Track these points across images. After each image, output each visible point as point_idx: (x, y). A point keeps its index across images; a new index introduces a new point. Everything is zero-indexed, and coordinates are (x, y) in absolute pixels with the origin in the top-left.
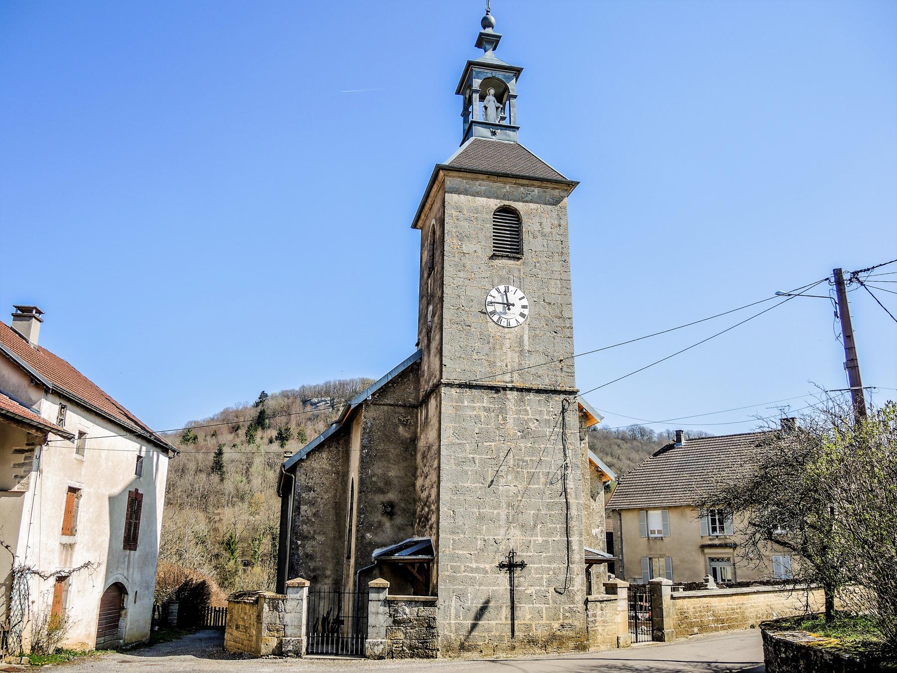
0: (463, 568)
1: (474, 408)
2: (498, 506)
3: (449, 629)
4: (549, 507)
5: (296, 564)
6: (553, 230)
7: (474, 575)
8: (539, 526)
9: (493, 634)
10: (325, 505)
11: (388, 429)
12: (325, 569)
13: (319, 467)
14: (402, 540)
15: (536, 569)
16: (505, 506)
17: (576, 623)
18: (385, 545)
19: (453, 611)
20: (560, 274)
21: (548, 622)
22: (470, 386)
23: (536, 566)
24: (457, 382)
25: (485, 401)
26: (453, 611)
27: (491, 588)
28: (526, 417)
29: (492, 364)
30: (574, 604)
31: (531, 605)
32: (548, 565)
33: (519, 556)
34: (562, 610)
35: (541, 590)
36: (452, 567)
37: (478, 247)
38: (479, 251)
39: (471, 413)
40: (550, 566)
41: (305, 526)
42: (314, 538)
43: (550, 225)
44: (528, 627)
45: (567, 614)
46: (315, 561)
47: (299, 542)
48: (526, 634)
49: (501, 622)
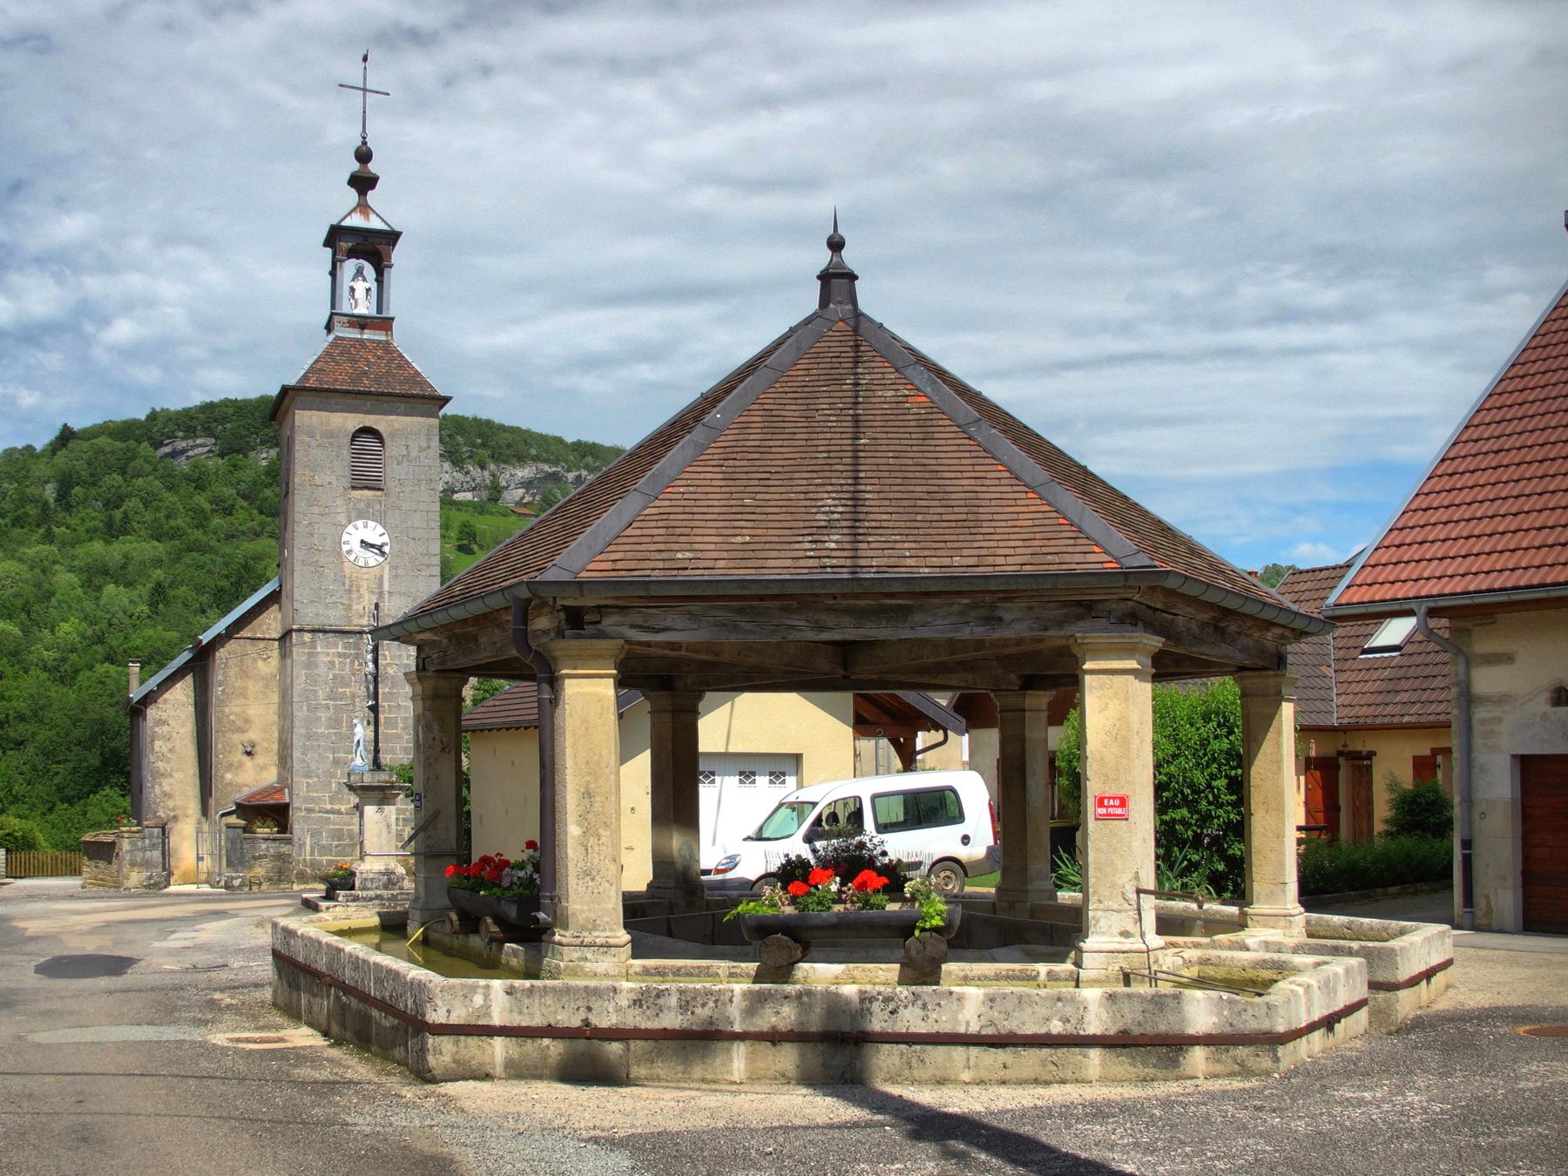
1: (328, 654)
10: (182, 739)
12: (186, 808)
19: (308, 848)
24: (310, 627)
26: (308, 848)
29: (349, 607)
37: (333, 479)
38: (334, 482)
41: (160, 763)
42: (171, 776)
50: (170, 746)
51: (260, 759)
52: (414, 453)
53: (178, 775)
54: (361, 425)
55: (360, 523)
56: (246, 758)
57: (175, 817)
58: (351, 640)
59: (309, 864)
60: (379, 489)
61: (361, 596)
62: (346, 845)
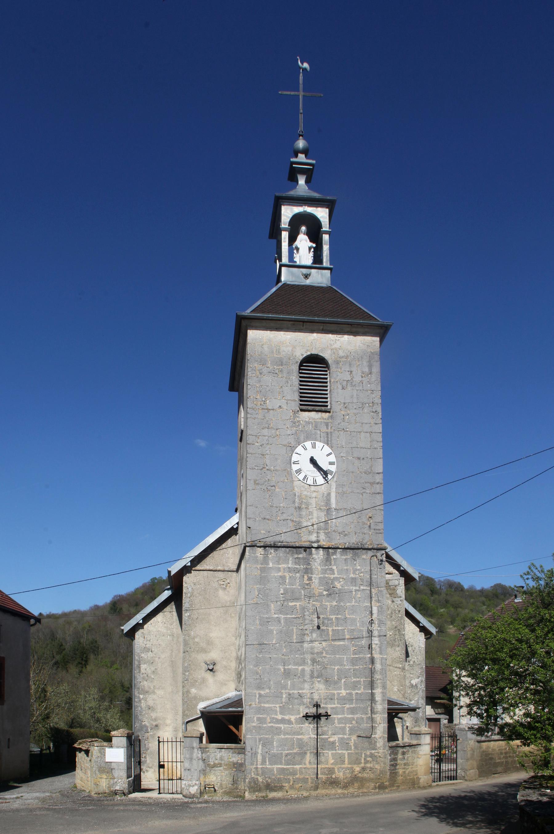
0: (268, 720)
1: (279, 570)
2: (303, 662)
3: (256, 773)
4: (354, 662)
5: (140, 714)
6: (364, 379)
7: (279, 725)
8: (343, 681)
9: (297, 776)
11: (208, 593)
13: (155, 630)
14: (225, 694)
15: (339, 719)
16: (309, 662)
17: (377, 766)
18: (208, 699)
19: (260, 757)
20: (371, 426)
21: (349, 766)
22: (275, 546)
23: (340, 716)
25: (290, 562)
26: (260, 757)
27: (296, 737)
28: (332, 576)
30: (376, 750)
31: (334, 752)
32: (350, 716)
33: (323, 708)
34: (363, 755)
35: (344, 738)
36: (259, 719)
37: (283, 403)
38: (285, 407)
39: (276, 575)
40: (352, 716)
41: (145, 682)
42: (154, 693)
43: (361, 374)
44: (331, 771)
45: (369, 759)
46: (157, 712)
47: (141, 696)
48: (329, 776)
49: (305, 766)
50: (153, 669)
51: (221, 676)
52: (357, 379)
53: (160, 692)
54: (309, 353)
55: (308, 444)
56: (209, 675)
57: (156, 726)
58: (301, 556)
59: (260, 772)
60: (326, 412)
61: (311, 513)
62: (296, 753)
